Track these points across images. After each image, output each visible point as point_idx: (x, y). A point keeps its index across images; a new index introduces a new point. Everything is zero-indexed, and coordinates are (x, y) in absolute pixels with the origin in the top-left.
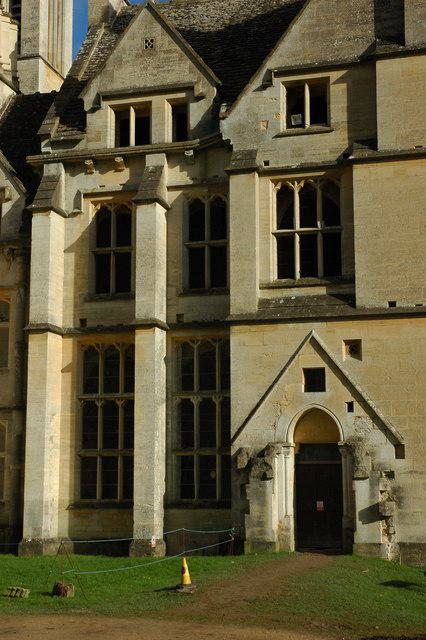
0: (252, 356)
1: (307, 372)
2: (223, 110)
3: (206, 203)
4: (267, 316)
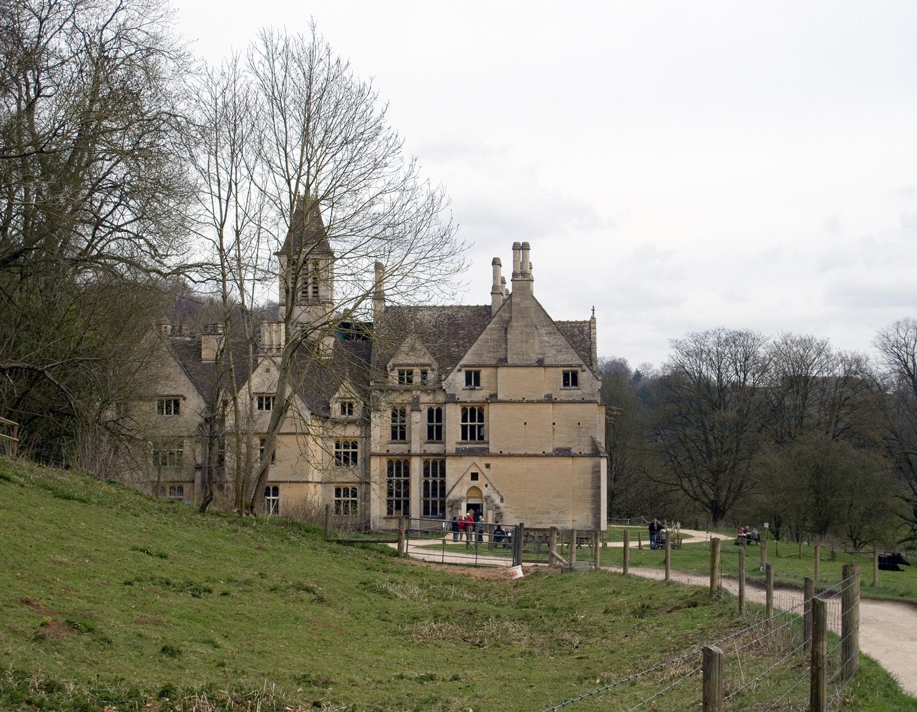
0: (455, 470)
1: (472, 474)
2: (443, 377)
3: (435, 409)
4: (459, 454)
